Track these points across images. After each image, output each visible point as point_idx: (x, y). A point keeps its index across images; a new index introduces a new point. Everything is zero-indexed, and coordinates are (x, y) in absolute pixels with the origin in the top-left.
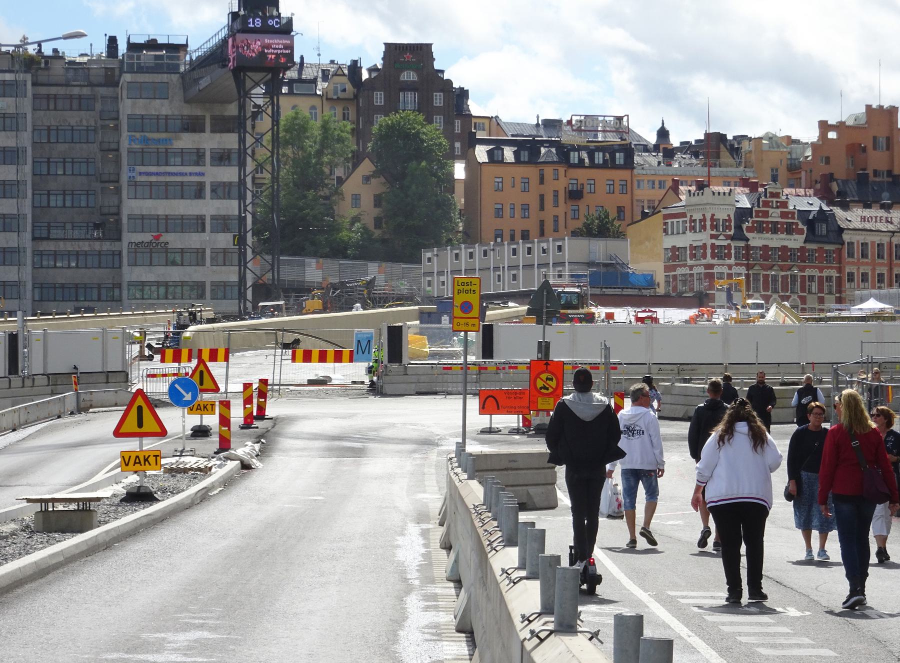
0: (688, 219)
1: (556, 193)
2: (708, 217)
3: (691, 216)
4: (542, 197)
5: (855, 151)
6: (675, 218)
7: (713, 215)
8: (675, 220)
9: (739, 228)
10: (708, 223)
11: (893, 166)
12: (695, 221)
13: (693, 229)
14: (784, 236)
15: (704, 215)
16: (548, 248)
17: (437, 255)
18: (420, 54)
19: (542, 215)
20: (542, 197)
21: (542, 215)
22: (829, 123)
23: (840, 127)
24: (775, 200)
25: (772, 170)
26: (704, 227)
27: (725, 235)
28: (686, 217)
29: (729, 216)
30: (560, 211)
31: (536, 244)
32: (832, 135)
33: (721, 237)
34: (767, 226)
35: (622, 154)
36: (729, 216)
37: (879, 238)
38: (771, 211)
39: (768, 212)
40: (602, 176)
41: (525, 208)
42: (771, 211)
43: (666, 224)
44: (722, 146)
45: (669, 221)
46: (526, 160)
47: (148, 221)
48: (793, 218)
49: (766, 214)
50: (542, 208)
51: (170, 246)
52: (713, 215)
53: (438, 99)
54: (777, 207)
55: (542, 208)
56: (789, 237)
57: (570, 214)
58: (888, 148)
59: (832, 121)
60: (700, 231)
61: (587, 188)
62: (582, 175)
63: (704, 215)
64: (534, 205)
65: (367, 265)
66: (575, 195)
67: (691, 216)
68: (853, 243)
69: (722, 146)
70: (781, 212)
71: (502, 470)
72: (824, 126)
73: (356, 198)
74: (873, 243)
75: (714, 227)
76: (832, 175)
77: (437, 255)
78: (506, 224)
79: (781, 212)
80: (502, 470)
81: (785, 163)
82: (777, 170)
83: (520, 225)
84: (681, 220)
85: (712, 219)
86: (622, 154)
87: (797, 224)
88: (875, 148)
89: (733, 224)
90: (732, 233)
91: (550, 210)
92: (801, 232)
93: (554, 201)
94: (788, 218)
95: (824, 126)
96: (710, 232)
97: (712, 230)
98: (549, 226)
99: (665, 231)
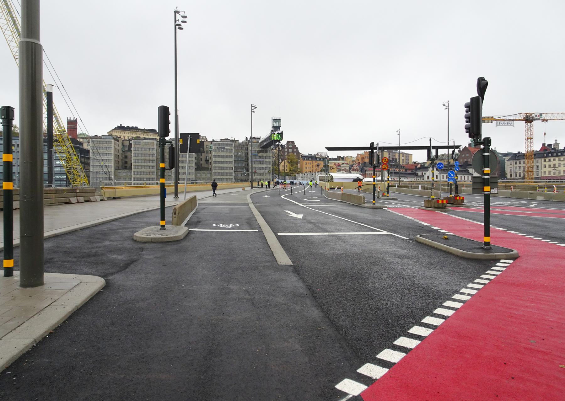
18: (293, 142)
53: (295, 150)
62: (319, 162)
66: (318, 166)
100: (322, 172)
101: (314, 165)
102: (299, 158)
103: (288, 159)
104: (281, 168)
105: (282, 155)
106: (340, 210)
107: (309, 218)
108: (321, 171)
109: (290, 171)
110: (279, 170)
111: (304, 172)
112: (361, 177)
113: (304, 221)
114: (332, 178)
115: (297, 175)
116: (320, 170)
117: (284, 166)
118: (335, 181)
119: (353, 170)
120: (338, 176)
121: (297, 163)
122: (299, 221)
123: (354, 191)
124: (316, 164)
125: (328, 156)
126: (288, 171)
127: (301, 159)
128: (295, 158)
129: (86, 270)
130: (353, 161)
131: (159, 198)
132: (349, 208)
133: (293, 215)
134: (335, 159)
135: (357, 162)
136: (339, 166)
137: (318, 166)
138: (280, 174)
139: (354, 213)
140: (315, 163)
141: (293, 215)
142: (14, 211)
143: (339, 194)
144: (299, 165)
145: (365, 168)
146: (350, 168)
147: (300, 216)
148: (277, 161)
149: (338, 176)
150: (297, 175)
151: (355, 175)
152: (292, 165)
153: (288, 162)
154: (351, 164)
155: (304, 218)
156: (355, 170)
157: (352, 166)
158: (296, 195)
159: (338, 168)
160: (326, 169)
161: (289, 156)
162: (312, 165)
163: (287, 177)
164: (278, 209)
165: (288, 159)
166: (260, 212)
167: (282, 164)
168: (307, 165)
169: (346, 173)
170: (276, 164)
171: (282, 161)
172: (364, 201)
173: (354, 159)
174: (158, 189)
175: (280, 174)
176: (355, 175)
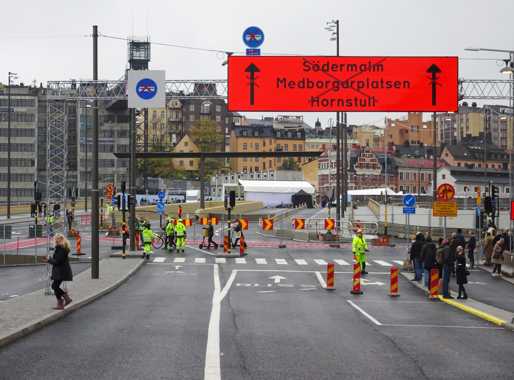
14: (371, 170)
24: (368, 154)
38: (366, 159)
42: (366, 159)
49: (364, 160)
54: (369, 157)
72: (484, 105)
76: (393, 143)
81: (372, 137)
84: (326, 162)
87: (377, 165)
92: (379, 168)
99: (319, 167)
135: (388, 140)
173: (378, 133)
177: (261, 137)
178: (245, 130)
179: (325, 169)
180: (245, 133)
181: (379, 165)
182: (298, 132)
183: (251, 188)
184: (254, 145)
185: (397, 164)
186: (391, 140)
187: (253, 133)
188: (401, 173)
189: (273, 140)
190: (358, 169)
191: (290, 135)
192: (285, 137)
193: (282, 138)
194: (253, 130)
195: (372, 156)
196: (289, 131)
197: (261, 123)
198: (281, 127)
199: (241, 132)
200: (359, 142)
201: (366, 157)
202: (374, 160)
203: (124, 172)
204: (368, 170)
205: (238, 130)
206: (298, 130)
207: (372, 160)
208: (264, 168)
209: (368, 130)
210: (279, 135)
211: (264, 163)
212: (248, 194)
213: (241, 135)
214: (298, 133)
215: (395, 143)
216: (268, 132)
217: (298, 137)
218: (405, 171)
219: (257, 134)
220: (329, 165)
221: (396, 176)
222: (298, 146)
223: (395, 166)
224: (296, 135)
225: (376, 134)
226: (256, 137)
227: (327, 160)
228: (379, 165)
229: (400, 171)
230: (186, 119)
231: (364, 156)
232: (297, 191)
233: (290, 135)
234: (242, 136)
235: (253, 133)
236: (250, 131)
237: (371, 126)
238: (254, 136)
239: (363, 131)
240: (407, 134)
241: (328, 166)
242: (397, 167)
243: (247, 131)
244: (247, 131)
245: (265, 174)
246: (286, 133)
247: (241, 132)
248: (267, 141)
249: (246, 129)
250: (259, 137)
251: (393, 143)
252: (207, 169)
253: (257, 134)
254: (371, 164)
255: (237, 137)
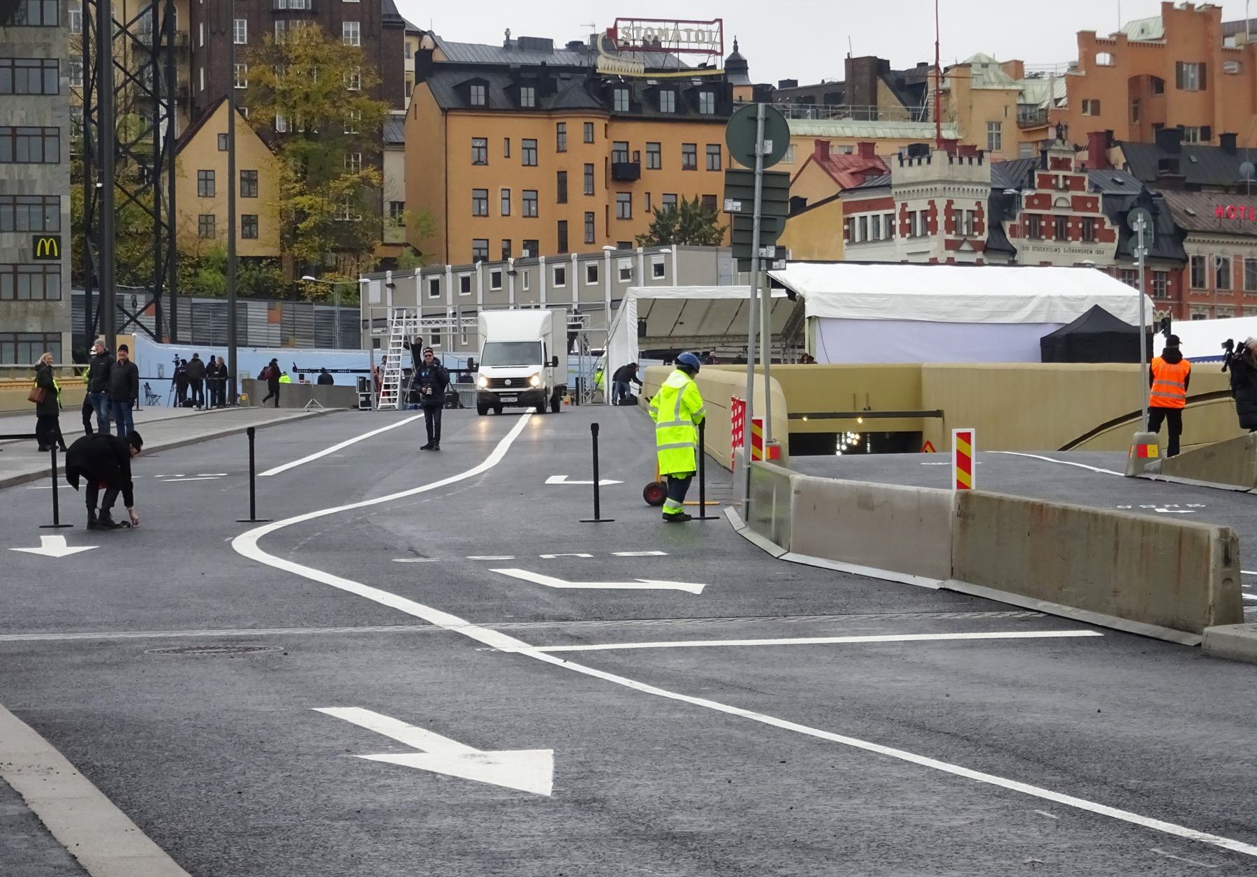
0: (897, 211)
1: (590, 168)
2: (941, 205)
3: (905, 205)
4: (562, 177)
5: (1146, 88)
6: (870, 208)
7: (950, 203)
8: (869, 214)
9: (996, 228)
10: (941, 219)
11: (1213, 120)
12: (912, 214)
13: (908, 230)
14: (1077, 244)
15: (932, 203)
16: (635, 270)
17: (392, 286)
19: (563, 212)
20: (562, 177)
21: (563, 212)
22: (1098, 36)
23: (1117, 43)
24: (1061, 173)
25: (990, 125)
26: (931, 227)
27: (971, 243)
28: (893, 206)
29: (978, 204)
30: (598, 203)
31: (575, 263)
32: (1103, 58)
33: (965, 247)
34: (1049, 224)
35: (711, 95)
36: (978, 204)
37: (1220, 248)
38: (1055, 195)
39: (1049, 196)
40: (673, 138)
41: (531, 197)
42: (1055, 195)
43: (849, 221)
44: (881, 82)
45: (857, 216)
46: (532, 104)
47: (25, 209)
48: (1095, 209)
49: (1045, 201)
50: (563, 198)
51: (1239, 143)
52: (950, 203)
54: (1066, 188)
55: (563, 198)
56: (1088, 246)
57: (616, 210)
58: (1203, 86)
59: (1102, 34)
60: (924, 235)
61: (645, 161)
62: (637, 135)
63: (932, 203)
64: (549, 191)
65: (245, 306)
66: (624, 173)
67: (905, 205)
68: (1202, 259)
69: (881, 82)
70: (1074, 198)
71: (1180, 548)
72: (1088, 40)
73: (206, 178)
74: (1238, 257)
75: (951, 226)
76: (1109, 133)
77: (392, 286)
78: (495, 230)
79: (1074, 198)
80: (1180, 548)
81: (1013, 112)
82: (999, 126)
83: (520, 230)
84: (882, 213)
85: (949, 211)
86: (711, 95)
87: (1101, 221)
88: (1180, 85)
89: (985, 220)
90: (984, 237)
91: (578, 202)
92: (1109, 237)
93: (587, 184)
94: (1086, 210)
95: (1088, 40)
96: (943, 234)
97: (949, 232)
98: (576, 233)
99: (848, 234)
100: (672, 254)
101: (574, 164)
102: (392, 90)
103: (267, 95)
104: (189, 204)
105: (191, 54)
106: (972, 695)
107: (639, 788)
108: (661, 235)
109: (290, 235)
110: (163, 232)
111: (462, 250)
112: (1126, 301)
113: (591, 825)
114: (793, 324)
115: (373, 290)
116: (643, 222)
117: (219, 179)
118: (831, 350)
119: (1035, 229)
120: (876, 296)
121: (374, 145)
122: (537, 828)
123: (1095, 479)
124: (600, 153)
125: (737, 65)
126: (264, 244)
127: (422, 99)
128: (352, 78)
129: (1032, 775)
130: (1032, 120)
131: (51, 479)
132: (1072, 669)
133: (441, 755)
134: (825, 99)
135: (1083, 127)
136: (868, 172)
137: (624, 173)
138: (167, 274)
139: (1136, 729)
140: (588, 144)
141: (441, 755)
142: (1227, 386)
143: (927, 511)
144: (394, 164)
145: (1174, 200)
146: (1002, 205)
147: (529, 771)
148: (130, 128)
149: (876, 296)
150: (373, 290)
151: (1074, 285)
152: (312, 173)
153: (267, 135)
154: (1012, 147)
155: (575, 793)
156: (1061, 230)
157: (1024, 173)
158: (408, 530)
159: (868, 203)
160: (758, 218)
161: (280, 58)
162: (550, 162)
163: (257, 311)
164: (233, 694)
165: (267, 95)
166: (47, 727)
167: (202, 153)
168: (498, 162)
169: (955, 253)
170: (121, 153)
171: (198, 119)
172: (1230, 581)
173: (1038, 94)
174: (27, 386)
175: (167, 274)
176: (1074, 285)
177: (550, 112)
178: (478, 82)
179: (876, 240)
180: (478, 95)
181: (1108, 226)
182: (701, 88)
183: (841, 299)
184: (516, 146)
185: (1177, 219)
186: (1100, 125)
187: (513, 94)
188: (1198, 260)
189: (599, 125)
190: (1025, 241)
191: (668, 102)
192: (648, 112)
193: (635, 115)
194: (507, 82)
195: (1077, 183)
196: (666, 84)
197: (502, 59)
198: (631, 67)
199: (462, 91)
200: (960, 131)
201: (1056, 187)
202: (1085, 199)
203: (22, 252)
204: (1062, 245)
205: (445, 83)
206: (698, 83)
207: (1078, 203)
208: (563, 246)
209: (993, 80)
210: (622, 101)
211: (563, 224)
212: (826, 327)
213: (462, 103)
214: (702, 95)
215: (1117, 137)
216: (574, 92)
217: (703, 110)
218: (1212, 248)
219: (528, 96)
220: (897, 222)
221: (1178, 275)
222: (702, 151)
223: (1171, 230)
224: (695, 103)
225: (1030, 100)
226: (621, 86)
227: (889, 203)
228: (1108, 226)
229: (1191, 249)
230: (210, 34)
231: (1046, 182)
232: (1069, 317)
233: (668, 102)
234: (466, 107)
235: (513, 94)
236: (498, 85)
237: (1005, 66)
238: (515, 108)
239: (976, 84)
240: (1158, 98)
241: (891, 230)
242: (1180, 235)
243: (486, 85)
244: (486, 85)
245: (625, 263)
246: (652, 95)
247: (462, 91)
248: (574, 127)
249: (488, 77)
250: (537, 110)
251: (1109, 133)
252: (322, 248)
253: (528, 96)
254: (1076, 220)
255: (445, 111)
